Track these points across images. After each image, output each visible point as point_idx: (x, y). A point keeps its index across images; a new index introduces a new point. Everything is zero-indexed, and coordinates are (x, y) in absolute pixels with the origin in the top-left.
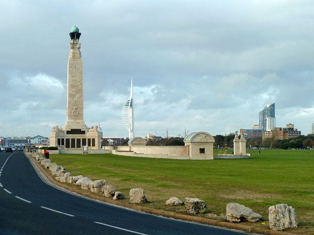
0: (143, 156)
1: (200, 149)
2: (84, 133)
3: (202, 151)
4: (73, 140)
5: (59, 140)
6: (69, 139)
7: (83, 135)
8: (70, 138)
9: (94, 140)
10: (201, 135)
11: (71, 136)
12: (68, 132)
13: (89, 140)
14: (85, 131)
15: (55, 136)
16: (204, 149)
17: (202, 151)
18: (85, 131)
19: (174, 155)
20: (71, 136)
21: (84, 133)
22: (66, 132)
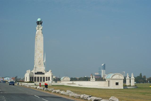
0: (82, 86)
1: (116, 85)
2: (44, 74)
3: (117, 84)
4: (38, 78)
5: (31, 77)
6: (43, 81)
7: (43, 75)
8: (37, 82)
9: (49, 78)
10: (117, 75)
11: (37, 76)
12: (36, 74)
13: (47, 77)
14: (44, 73)
15: (29, 75)
16: (116, 85)
17: (117, 84)
18: (44, 73)
19: (101, 86)
20: (37, 76)
21: (44, 74)
22: (34, 74)
